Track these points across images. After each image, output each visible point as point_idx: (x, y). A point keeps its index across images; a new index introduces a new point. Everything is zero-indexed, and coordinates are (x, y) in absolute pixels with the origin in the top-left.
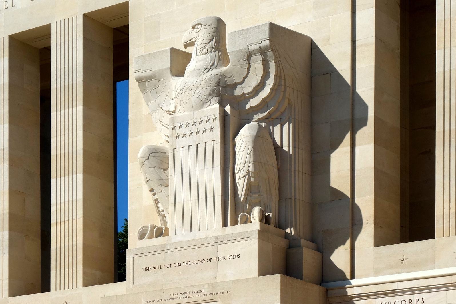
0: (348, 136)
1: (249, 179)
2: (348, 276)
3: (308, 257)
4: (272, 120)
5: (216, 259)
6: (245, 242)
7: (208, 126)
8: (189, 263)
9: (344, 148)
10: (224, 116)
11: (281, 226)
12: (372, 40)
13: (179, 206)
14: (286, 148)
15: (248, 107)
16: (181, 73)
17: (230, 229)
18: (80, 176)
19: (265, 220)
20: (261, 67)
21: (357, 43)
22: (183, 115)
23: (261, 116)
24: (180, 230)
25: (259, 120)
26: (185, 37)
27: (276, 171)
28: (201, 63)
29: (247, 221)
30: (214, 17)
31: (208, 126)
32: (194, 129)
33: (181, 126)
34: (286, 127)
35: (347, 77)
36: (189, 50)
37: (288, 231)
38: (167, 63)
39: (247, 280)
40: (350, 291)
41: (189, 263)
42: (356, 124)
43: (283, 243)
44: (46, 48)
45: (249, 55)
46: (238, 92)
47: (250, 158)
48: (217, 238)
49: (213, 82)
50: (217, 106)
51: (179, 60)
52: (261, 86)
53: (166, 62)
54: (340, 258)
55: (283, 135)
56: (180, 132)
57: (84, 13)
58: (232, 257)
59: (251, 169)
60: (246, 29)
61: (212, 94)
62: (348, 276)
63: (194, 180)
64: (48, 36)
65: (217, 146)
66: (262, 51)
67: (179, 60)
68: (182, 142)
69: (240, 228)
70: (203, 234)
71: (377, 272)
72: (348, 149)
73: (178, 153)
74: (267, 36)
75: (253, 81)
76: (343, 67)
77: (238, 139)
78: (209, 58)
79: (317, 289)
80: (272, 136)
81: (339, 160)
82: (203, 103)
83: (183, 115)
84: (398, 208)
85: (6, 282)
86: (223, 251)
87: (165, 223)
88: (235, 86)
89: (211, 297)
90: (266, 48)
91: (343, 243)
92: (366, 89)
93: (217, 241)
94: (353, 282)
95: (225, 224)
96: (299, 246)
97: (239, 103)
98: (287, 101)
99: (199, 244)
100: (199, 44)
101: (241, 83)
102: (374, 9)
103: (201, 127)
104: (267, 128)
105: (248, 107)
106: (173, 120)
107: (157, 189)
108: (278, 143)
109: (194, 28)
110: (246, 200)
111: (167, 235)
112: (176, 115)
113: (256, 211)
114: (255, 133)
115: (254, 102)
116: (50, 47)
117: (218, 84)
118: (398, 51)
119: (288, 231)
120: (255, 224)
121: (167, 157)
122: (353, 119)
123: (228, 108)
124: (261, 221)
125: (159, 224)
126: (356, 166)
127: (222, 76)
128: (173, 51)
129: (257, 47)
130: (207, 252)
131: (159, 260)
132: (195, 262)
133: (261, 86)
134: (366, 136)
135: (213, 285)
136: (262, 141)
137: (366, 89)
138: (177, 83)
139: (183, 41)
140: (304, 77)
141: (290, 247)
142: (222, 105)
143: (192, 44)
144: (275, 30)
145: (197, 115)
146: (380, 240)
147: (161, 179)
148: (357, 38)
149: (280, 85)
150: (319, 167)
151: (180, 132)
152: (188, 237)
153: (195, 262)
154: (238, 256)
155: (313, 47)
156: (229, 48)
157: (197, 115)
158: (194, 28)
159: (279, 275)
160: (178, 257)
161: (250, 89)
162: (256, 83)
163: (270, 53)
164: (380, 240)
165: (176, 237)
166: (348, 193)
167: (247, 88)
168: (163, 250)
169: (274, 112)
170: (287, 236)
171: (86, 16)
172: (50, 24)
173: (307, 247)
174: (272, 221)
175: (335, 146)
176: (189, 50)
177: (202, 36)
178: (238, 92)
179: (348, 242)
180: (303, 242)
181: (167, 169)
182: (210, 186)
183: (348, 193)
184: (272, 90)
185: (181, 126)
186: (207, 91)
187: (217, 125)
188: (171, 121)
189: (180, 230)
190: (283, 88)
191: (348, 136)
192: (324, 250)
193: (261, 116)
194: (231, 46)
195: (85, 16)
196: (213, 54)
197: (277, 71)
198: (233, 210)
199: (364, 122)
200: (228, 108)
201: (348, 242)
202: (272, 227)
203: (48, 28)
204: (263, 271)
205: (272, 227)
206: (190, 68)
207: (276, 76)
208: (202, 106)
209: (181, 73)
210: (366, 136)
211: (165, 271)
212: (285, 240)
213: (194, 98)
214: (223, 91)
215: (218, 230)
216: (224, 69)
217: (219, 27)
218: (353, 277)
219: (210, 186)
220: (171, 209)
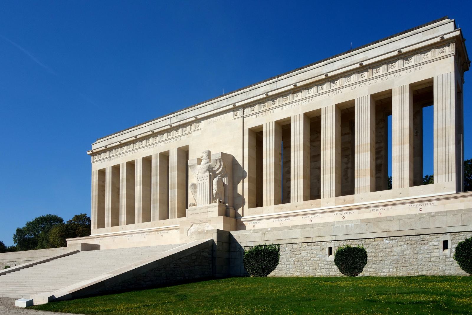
0: (242, 180)
1: (216, 191)
2: (242, 216)
3: (231, 211)
4: (222, 176)
5: (208, 212)
6: (215, 208)
7: (206, 178)
8: (201, 213)
9: (241, 183)
10: (210, 176)
11: (224, 203)
12: (248, 156)
13: (199, 198)
14: (226, 184)
15: (216, 173)
16: (200, 165)
17: (211, 204)
18: (177, 189)
19: (220, 202)
20: (219, 163)
21: (244, 157)
22: (200, 175)
23: (219, 175)
24: (199, 204)
25: (219, 176)
26: (201, 156)
27: (223, 190)
28: (204, 162)
29: (216, 202)
30: (207, 151)
31: (206, 178)
32: (203, 179)
33: (199, 178)
34: (226, 178)
35: (242, 165)
36: (202, 158)
37: (226, 204)
38: (196, 162)
39: (215, 217)
40: (242, 220)
41: (201, 213)
42: (244, 177)
43: (225, 208)
44: (289, 124)
45: (216, 160)
46: (214, 169)
47: (216, 186)
48: (208, 206)
49: (207, 167)
50: (208, 173)
51: (199, 161)
52: (219, 168)
53: (196, 162)
54: (240, 211)
55: (225, 180)
56: (199, 179)
57: (305, 112)
58: (211, 212)
59: (216, 189)
60: (216, 154)
61: (207, 170)
62: (242, 216)
63: (203, 192)
64: (290, 120)
65: (208, 183)
66: (219, 159)
67: (199, 161)
68: (200, 182)
69: (214, 204)
70: (205, 206)
71: (249, 215)
72: (242, 184)
73: (199, 185)
74: (220, 156)
75: (217, 167)
76: (240, 163)
77: (213, 181)
78: (206, 161)
79: (234, 220)
80: (222, 180)
81: (240, 186)
82: (205, 172)
83: (200, 175)
84: (255, 198)
85: (158, 216)
86: (209, 210)
87: (196, 202)
88: (213, 168)
89: (206, 222)
90: (220, 159)
91: (241, 208)
92: (246, 169)
93: (208, 207)
94: (243, 217)
95: (210, 203)
96: (229, 209)
97: (214, 172)
98: (226, 172)
99: (204, 208)
100: (204, 157)
101: (214, 167)
102: (248, 148)
103: (204, 178)
104: (221, 178)
105: (216, 173)
106: (197, 176)
107: (194, 194)
108: (224, 182)
109: (203, 153)
110: (216, 197)
111: (196, 206)
112: (198, 175)
113: (218, 200)
114: (217, 180)
115: (218, 172)
116: (321, 116)
117: (208, 168)
118: (255, 158)
119: (226, 204)
120: (217, 203)
121: (196, 186)
122: (243, 176)
123: (211, 174)
124: (219, 202)
125: (195, 203)
126: (244, 188)
127: (210, 165)
128: (198, 159)
129: (218, 158)
130: (205, 210)
131: (194, 212)
132: (203, 213)
133: (219, 168)
134: (246, 180)
135: (207, 219)
136: (219, 182)
137: (246, 169)
138: (199, 167)
139: (200, 156)
140: (231, 165)
141: (227, 209)
142: (209, 173)
143: (203, 157)
144: (222, 154)
145: (204, 175)
146: (250, 207)
147: (195, 191)
148: (244, 155)
149: (224, 168)
150: (235, 188)
151: (199, 179)
152: (201, 206)
153: (203, 213)
154: (213, 211)
155: (233, 157)
156: (212, 159)
157: (204, 175)
158: (203, 153)
159: (223, 216)
160: (198, 211)
161: (217, 169)
162: (218, 167)
163: (221, 160)
164: (250, 207)
165: (198, 206)
166: (242, 195)
167: (216, 168)
168: (195, 209)
169: (223, 174)
170: (226, 206)
171: (178, 148)
172: (354, 100)
173: (231, 209)
174: (222, 202)
175: (238, 183)
176: (202, 158)
177: (205, 155)
178: (214, 169)
179: (242, 207)
180: (230, 207)
181: (196, 189)
182: (206, 193)
183: (242, 195)
184: (222, 169)
185: (199, 178)
186: (206, 169)
187: (208, 178)
188: (198, 176)
189: (199, 204)
190: (225, 168)
191: (242, 180)
192: (236, 209)
193: (219, 175)
194: (213, 158)
195: (178, 148)
196: (207, 160)
197: (223, 164)
198: (212, 199)
199: (246, 177)
200: (211, 174)
201: (242, 207)
202: (222, 204)
203: (354, 100)
204: (219, 215)
205: (222, 204)
206: (202, 163)
207: (223, 165)
208: (205, 173)
209: (200, 165)
210: (246, 180)
211: (196, 215)
212: (225, 207)
213: (203, 171)
214: (210, 169)
215: (208, 205)
216: (210, 163)
217: (209, 153)
218: (243, 216)
219: (206, 193)
220: (197, 199)
